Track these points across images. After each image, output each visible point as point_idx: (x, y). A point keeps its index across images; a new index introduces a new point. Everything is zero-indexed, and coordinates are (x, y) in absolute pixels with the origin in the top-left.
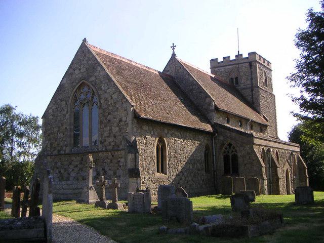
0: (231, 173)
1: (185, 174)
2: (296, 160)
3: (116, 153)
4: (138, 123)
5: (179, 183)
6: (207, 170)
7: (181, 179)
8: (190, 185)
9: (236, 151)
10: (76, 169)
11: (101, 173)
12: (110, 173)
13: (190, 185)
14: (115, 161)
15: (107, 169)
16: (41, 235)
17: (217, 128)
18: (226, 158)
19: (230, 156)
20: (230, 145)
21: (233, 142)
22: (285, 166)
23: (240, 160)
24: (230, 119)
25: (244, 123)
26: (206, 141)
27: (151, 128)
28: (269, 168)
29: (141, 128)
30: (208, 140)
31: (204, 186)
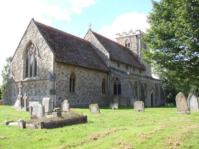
0: (117, 93)
1: (89, 94)
2: (159, 91)
3: (45, 81)
4: (58, 64)
5: (84, 99)
6: (104, 92)
7: (86, 97)
8: (92, 100)
9: (120, 82)
10: (26, 90)
11: (38, 92)
12: (42, 92)
13: (92, 100)
14: (45, 85)
15: (40, 89)
16: (100, 110)
17: (110, 70)
18: (115, 86)
19: (117, 85)
20: (117, 79)
21: (118, 77)
22: (151, 92)
23: (122, 87)
24: (120, 65)
25: (129, 67)
26: (103, 76)
27: (66, 68)
28: (140, 92)
29: (60, 67)
30: (105, 76)
31: (101, 101)
